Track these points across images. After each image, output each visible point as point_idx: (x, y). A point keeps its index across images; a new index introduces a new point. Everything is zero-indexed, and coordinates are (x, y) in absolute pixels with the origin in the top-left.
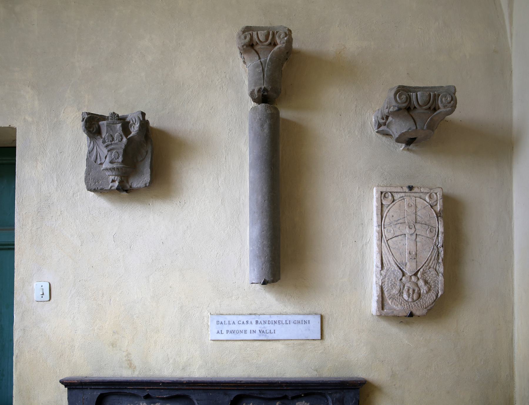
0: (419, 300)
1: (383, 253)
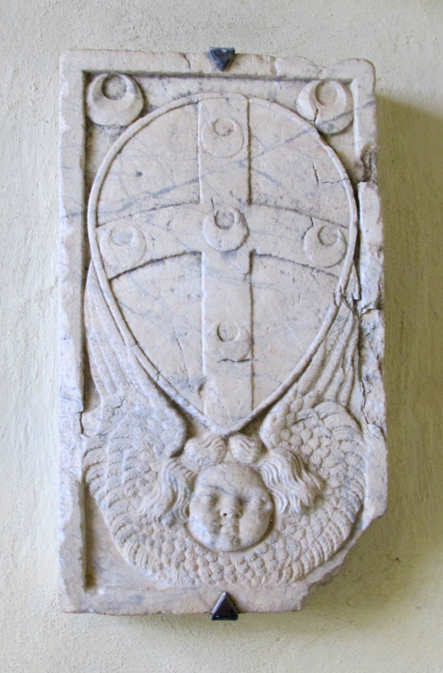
0: (268, 541)
1: (89, 337)
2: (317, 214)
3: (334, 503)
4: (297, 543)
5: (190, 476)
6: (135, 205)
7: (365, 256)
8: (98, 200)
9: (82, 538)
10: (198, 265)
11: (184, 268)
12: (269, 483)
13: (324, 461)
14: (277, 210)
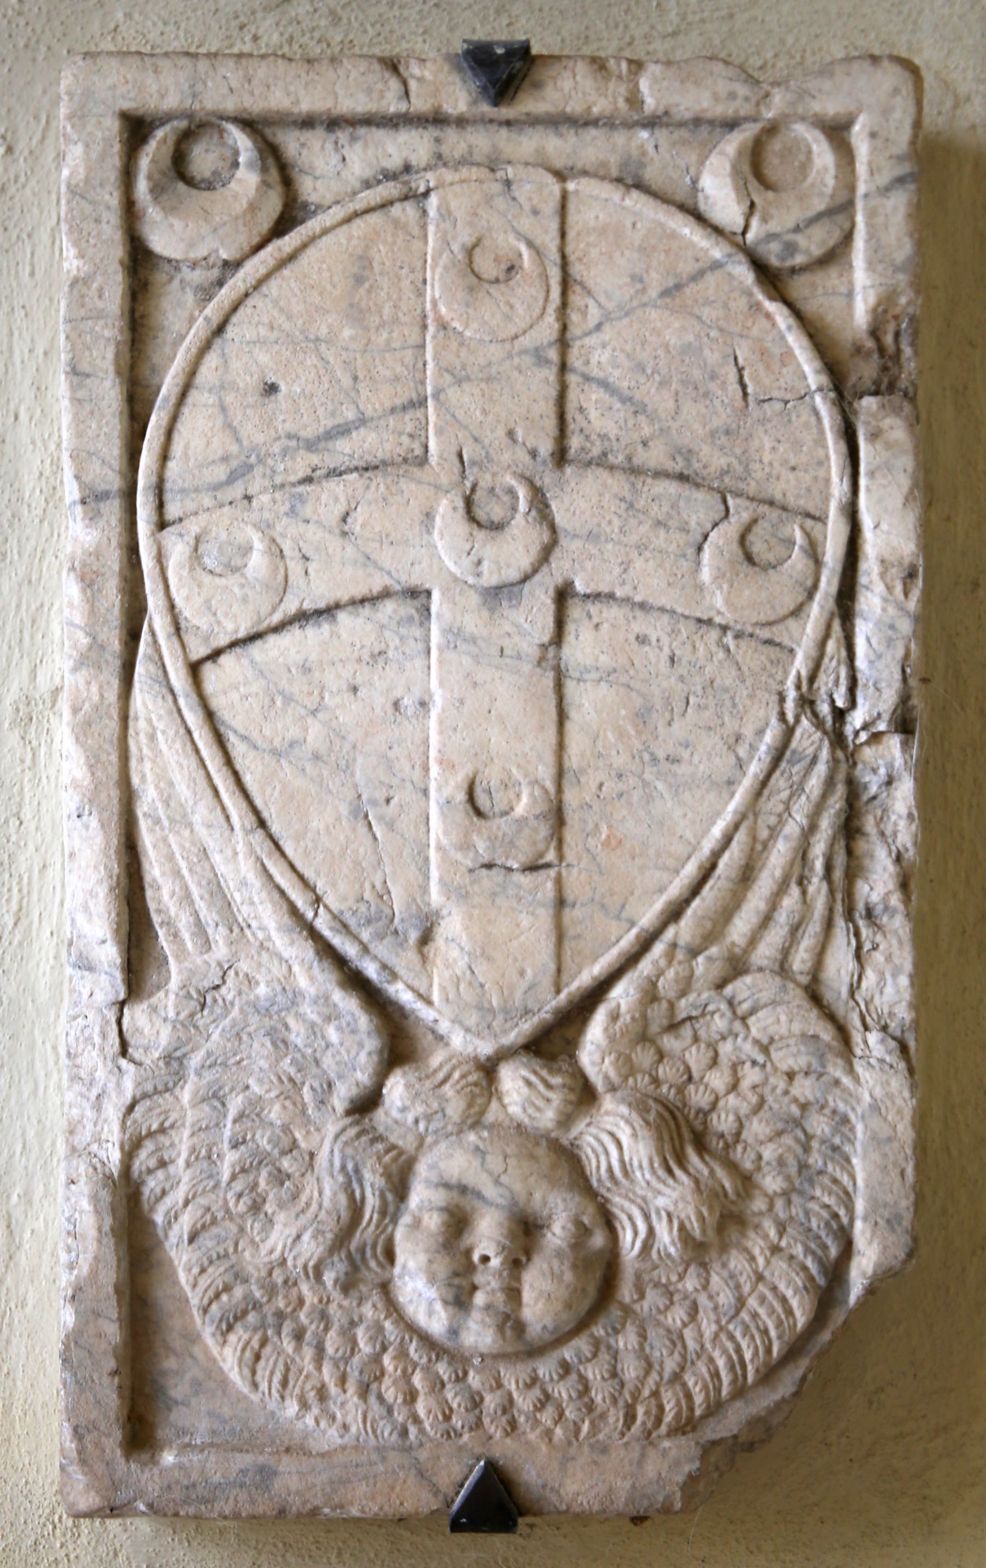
0: (599, 1330)
1: (141, 810)
2: (742, 485)
3: (773, 1233)
4: (675, 1337)
5: (395, 1159)
6: (259, 470)
7: (869, 594)
8: (164, 457)
9: (119, 1319)
10: (421, 624)
11: (387, 634)
12: (599, 1180)
13: (747, 1124)
14: (632, 478)
